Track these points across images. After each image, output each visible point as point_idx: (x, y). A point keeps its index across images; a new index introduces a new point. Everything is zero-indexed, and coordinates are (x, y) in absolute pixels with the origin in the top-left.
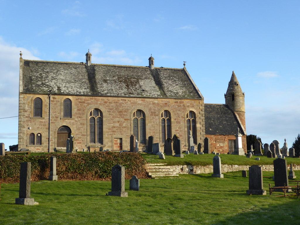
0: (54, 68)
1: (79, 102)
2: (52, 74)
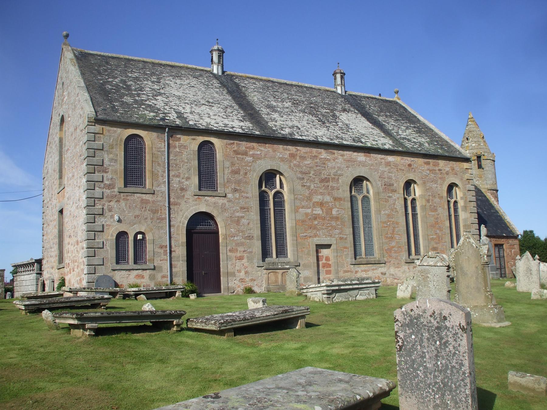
0: (148, 72)
1: (234, 151)
2: (150, 83)
